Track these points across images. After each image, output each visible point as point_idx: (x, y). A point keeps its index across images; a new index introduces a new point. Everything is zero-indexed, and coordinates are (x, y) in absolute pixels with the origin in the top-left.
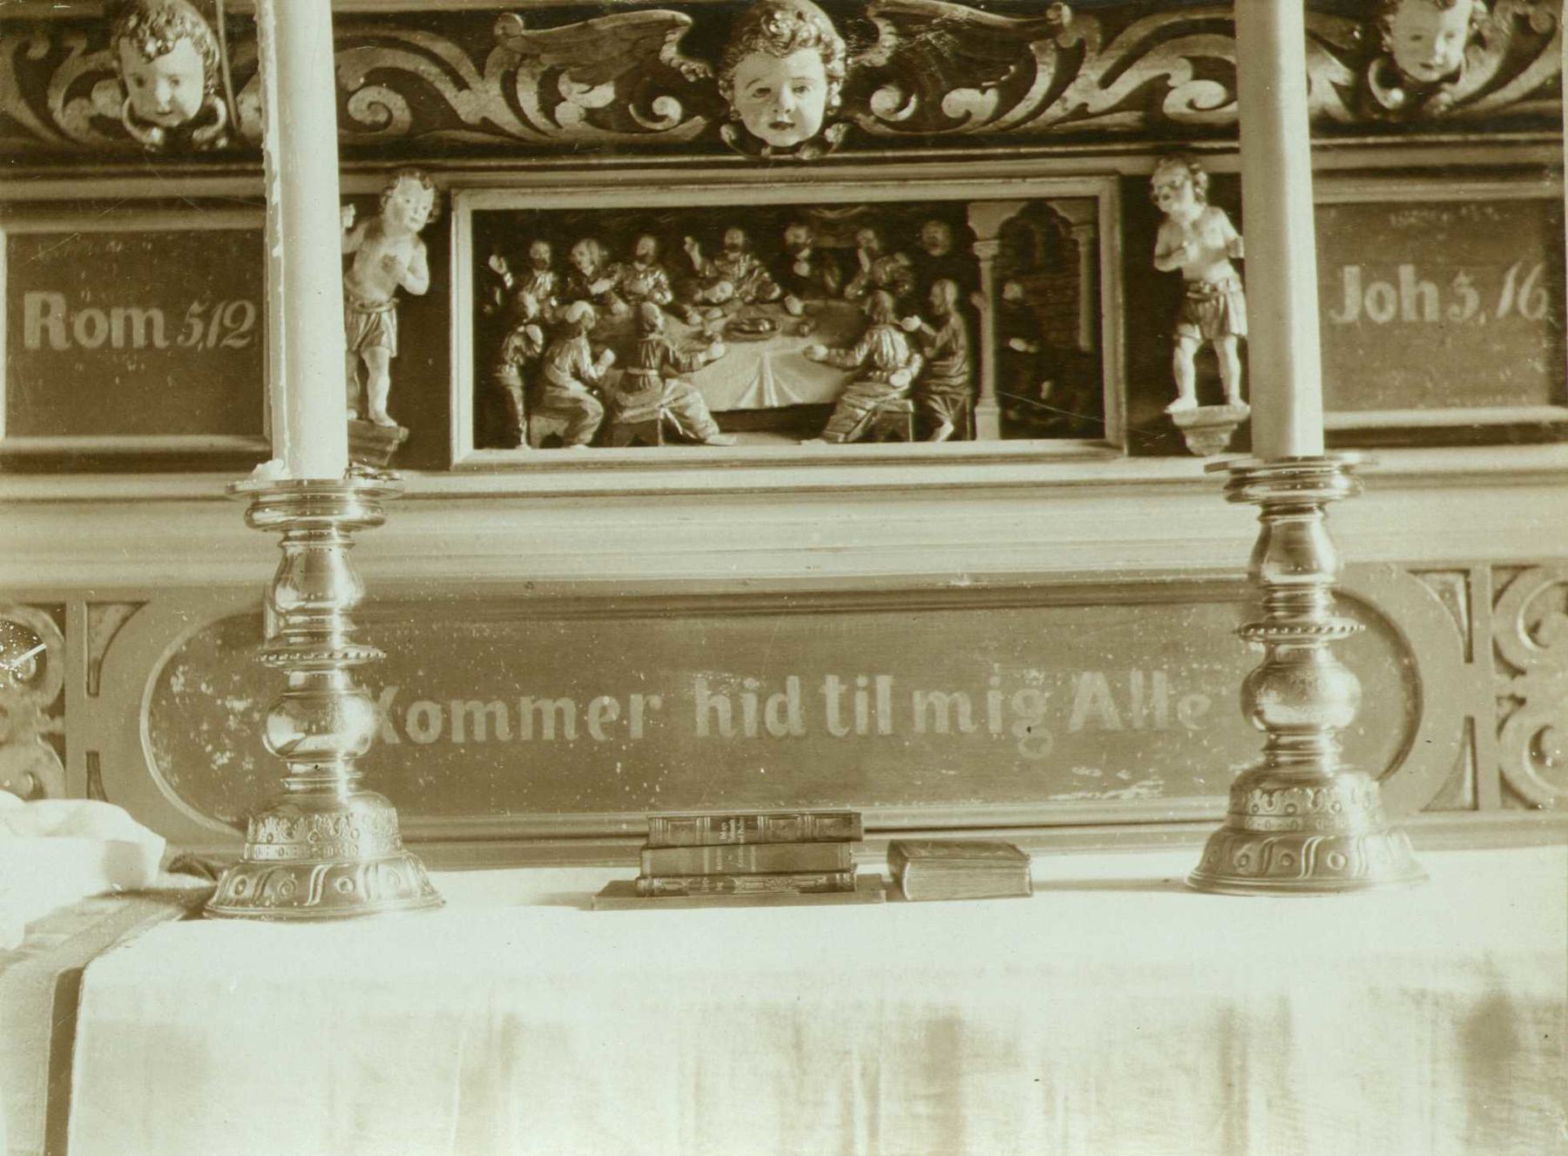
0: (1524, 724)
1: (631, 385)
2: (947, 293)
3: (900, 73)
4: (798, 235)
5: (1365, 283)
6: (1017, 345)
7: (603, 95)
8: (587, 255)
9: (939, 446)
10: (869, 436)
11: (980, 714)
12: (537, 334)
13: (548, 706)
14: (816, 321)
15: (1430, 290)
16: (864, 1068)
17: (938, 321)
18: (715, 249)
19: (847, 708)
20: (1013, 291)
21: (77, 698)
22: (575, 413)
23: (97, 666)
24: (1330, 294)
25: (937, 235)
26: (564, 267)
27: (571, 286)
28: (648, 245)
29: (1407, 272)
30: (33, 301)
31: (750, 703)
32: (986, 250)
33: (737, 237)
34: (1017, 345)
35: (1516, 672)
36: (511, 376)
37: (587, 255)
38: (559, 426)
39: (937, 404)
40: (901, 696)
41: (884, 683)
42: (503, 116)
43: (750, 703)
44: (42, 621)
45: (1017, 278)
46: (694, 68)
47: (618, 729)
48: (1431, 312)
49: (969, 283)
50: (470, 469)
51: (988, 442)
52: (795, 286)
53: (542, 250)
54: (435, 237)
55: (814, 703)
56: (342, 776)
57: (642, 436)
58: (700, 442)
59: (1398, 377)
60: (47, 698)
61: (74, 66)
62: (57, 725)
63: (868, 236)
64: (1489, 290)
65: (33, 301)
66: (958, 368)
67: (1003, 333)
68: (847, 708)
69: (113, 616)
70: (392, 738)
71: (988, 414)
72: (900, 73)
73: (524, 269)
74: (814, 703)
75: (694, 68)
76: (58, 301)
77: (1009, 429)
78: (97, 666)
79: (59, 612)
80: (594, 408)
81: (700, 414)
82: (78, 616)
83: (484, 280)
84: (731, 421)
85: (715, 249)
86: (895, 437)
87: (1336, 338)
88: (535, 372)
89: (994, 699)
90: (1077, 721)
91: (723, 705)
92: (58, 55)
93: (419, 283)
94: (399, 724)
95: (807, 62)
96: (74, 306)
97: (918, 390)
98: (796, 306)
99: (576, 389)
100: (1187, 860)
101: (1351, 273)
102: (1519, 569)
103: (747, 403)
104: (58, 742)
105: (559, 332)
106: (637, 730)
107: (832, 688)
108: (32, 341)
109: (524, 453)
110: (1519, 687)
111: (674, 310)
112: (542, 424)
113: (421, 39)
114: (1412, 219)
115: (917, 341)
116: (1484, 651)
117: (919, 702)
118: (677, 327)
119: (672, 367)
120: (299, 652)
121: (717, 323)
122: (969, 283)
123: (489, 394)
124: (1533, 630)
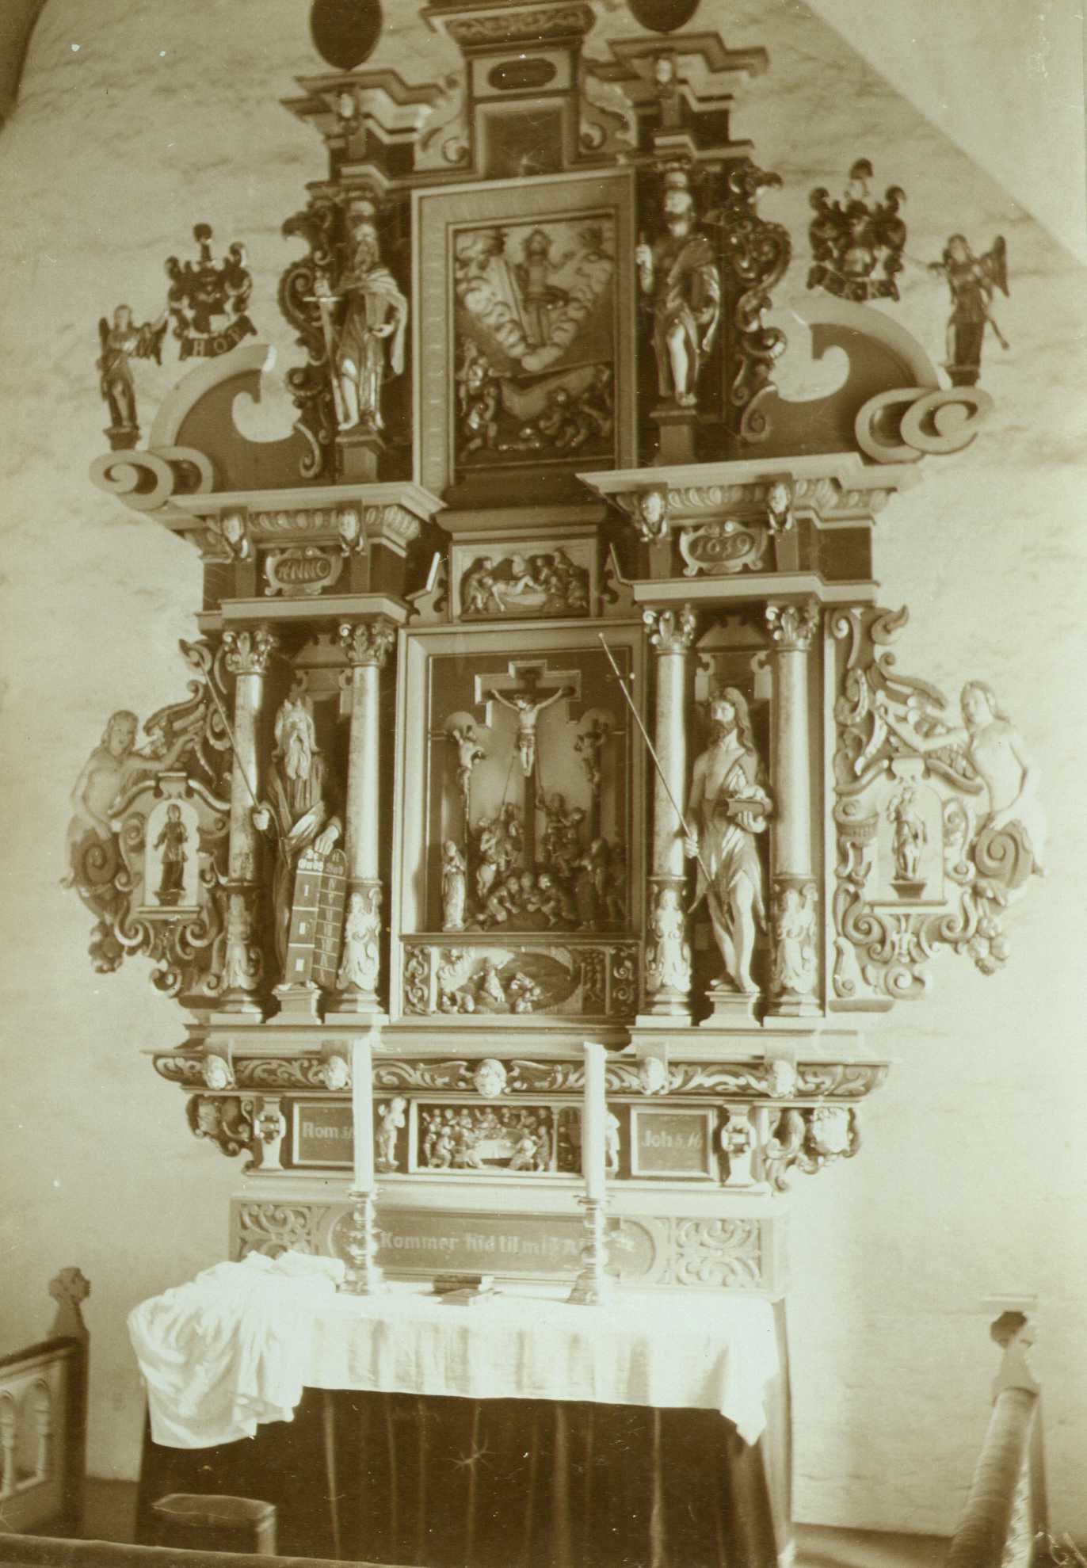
0: (683, 1262)
3: (522, 1078)
4: (505, 1111)
5: (652, 1134)
6: (562, 1145)
7: (446, 1080)
8: (449, 1114)
9: (540, 1172)
10: (520, 1169)
11: (540, 1249)
12: (434, 1137)
14: (509, 1134)
17: (540, 1137)
18: (483, 1113)
19: (506, 1244)
20: (562, 1130)
21: (314, 1231)
22: (443, 1159)
23: (318, 1223)
24: (642, 1138)
25: (543, 1113)
26: (443, 1116)
29: (663, 1134)
32: (555, 1117)
34: (562, 1145)
35: (680, 1246)
37: (449, 1114)
38: (439, 1162)
39: (539, 1161)
40: (520, 1242)
41: (516, 1239)
42: (421, 1083)
44: (305, 1211)
45: (564, 1126)
46: (469, 1075)
47: (447, 1248)
48: (670, 1145)
49: (550, 1127)
50: (414, 1174)
51: (553, 1172)
54: (406, 1112)
56: (370, 1262)
57: (460, 1166)
59: (660, 1162)
61: (314, 1069)
62: (309, 1238)
64: (686, 1139)
65: (305, 1124)
66: (546, 1150)
67: (559, 1141)
68: (506, 1244)
69: (322, 1210)
70: (390, 1246)
71: (553, 1163)
72: (522, 1078)
73: (432, 1116)
74: (497, 1243)
75: (469, 1075)
76: (311, 1125)
77: (561, 1168)
78: (318, 1223)
80: (448, 1156)
81: (477, 1159)
82: (314, 1209)
83: (421, 1120)
84: (486, 1162)
85: (483, 1113)
86: (528, 1169)
87: (643, 1151)
88: (434, 1146)
89: (544, 1246)
92: (311, 1066)
94: (392, 1242)
96: (315, 1126)
97: (534, 1157)
98: (504, 1130)
100: (566, 1293)
101: (648, 1133)
104: (308, 1242)
105: (439, 1135)
106: (452, 1247)
108: (305, 1135)
111: (471, 1130)
112: (435, 1161)
113: (400, 1064)
114: (665, 1118)
115: (535, 1143)
121: (483, 1133)
122: (550, 1127)
124: (687, 1236)
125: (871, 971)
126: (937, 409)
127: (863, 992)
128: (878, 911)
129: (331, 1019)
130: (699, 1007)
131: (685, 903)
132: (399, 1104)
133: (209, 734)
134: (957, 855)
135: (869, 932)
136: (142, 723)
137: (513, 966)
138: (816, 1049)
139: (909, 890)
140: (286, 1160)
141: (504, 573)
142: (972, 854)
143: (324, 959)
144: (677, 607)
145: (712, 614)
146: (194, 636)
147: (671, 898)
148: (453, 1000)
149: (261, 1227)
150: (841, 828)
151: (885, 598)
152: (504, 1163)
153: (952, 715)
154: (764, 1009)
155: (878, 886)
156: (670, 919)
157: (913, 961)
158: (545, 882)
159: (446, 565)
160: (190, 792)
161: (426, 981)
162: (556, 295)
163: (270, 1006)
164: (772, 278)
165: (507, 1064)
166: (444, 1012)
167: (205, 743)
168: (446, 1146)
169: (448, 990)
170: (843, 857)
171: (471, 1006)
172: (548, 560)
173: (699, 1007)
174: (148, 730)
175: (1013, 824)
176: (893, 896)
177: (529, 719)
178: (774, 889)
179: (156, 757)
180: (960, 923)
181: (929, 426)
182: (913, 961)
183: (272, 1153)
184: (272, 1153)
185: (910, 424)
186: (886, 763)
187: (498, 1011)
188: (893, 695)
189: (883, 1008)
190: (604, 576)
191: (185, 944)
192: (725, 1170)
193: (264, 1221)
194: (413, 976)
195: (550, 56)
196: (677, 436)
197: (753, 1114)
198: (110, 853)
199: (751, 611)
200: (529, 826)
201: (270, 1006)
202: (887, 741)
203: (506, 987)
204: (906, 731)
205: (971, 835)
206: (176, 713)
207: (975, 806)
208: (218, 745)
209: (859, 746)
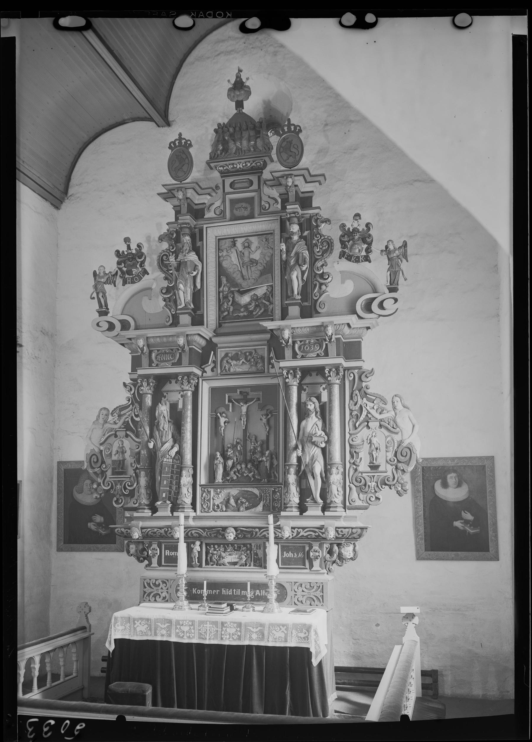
0: (297, 597)
1: (219, 560)
2: (249, 552)
4: (236, 545)
9: (247, 567)
10: (241, 566)
13: (209, 591)
15: (292, 554)
16: (177, 591)
22: (214, 562)
26: (214, 547)
27: (215, 550)
28: (222, 546)
30: (166, 551)
31: (227, 591)
33: (230, 545)
35: (296, 592)
36: (209, 558)
37: (216, 547)
38: (213, 563)
39: (247, 563)
43: (227, 591)
51: (252, 567)
52: (235, 550)
53: (212, 546)
54: (201, 546)
55: (233, 592)
58: (226, 565)
60: (167, 588)
63: (242, 546)
69: (172, 581)
73: (210, 547)
74: (233, 592)
79: (168, 580)
80: (216, 562)
82: (169, 581)
86: (243, 566)
88: (211, 558)
90: (256, 595)
91: (225, 591)
93: (199, 550)
95: (231, 534)
96: (170, 552)
97: (246, 561)
98: (235, 552)
99: (215, 560)
102: (297, 582)
103: (231, 561)
104: (167, 592)
107: (235, 590)
108: (166, 555)
109: (210, 566)
110: (296, 593)
112: (211, 563)
115: (246, 556)
116: (293, 590)
117: (242, 592)
118: (224, 554)
119: (223, 558)
120: (258, 538)
123: (206, 560)
125: (361, 495)
127: (358, 503)
128: (364, 475)
130: (302, 508)
131: (297, 472)
132: (198, 543)
133: (133, 416)
134: (390, 455)
135: (361, 482)
136: (111, 412)
138: (341, 523)
139: (374, 467)
140: (160, 564)
142: (396, 455)
144: (294, 369)
145: (306, 371)
146: (128, 381)
147: (292, 470)
148: (218, 506)
150: (351, 446)
151: (366, 366)
153: (389, 406)
154: (324, 509)
155: (364, 466)
156: (292, 478)
157: (376, 492)
158: (249, 466)
159: (215, 354)
160: (127, 436)
161: (209, 500)
162: (253, 262)
163: (154, 510)
165: (236, 529)
166: (215, 511)
168: (215, 558)
170: (352, 456)
172: (251, 353)
173: (302, 508)
176: (369, 469)
177: (244, 409)
178: (327, 471)
179: (115, 423)
180: (391, 479)
181: (381, 306)
183: (155, 561)
184: (155, 561)
185: (375, 306)
188: (369, 400)
189: (366, 508)
190: (270, 359)
191: (125, 488)
192: (311, 566)
195: (251, 177)
196: (294, 310)
197: (321, 546)
199: (320, 370)
200: (245, 446)
201: (154, 510)
202: (367, 415)
204: (373, 412)
206: (122, 408)
207: (397, 438)
209: (358, 418)
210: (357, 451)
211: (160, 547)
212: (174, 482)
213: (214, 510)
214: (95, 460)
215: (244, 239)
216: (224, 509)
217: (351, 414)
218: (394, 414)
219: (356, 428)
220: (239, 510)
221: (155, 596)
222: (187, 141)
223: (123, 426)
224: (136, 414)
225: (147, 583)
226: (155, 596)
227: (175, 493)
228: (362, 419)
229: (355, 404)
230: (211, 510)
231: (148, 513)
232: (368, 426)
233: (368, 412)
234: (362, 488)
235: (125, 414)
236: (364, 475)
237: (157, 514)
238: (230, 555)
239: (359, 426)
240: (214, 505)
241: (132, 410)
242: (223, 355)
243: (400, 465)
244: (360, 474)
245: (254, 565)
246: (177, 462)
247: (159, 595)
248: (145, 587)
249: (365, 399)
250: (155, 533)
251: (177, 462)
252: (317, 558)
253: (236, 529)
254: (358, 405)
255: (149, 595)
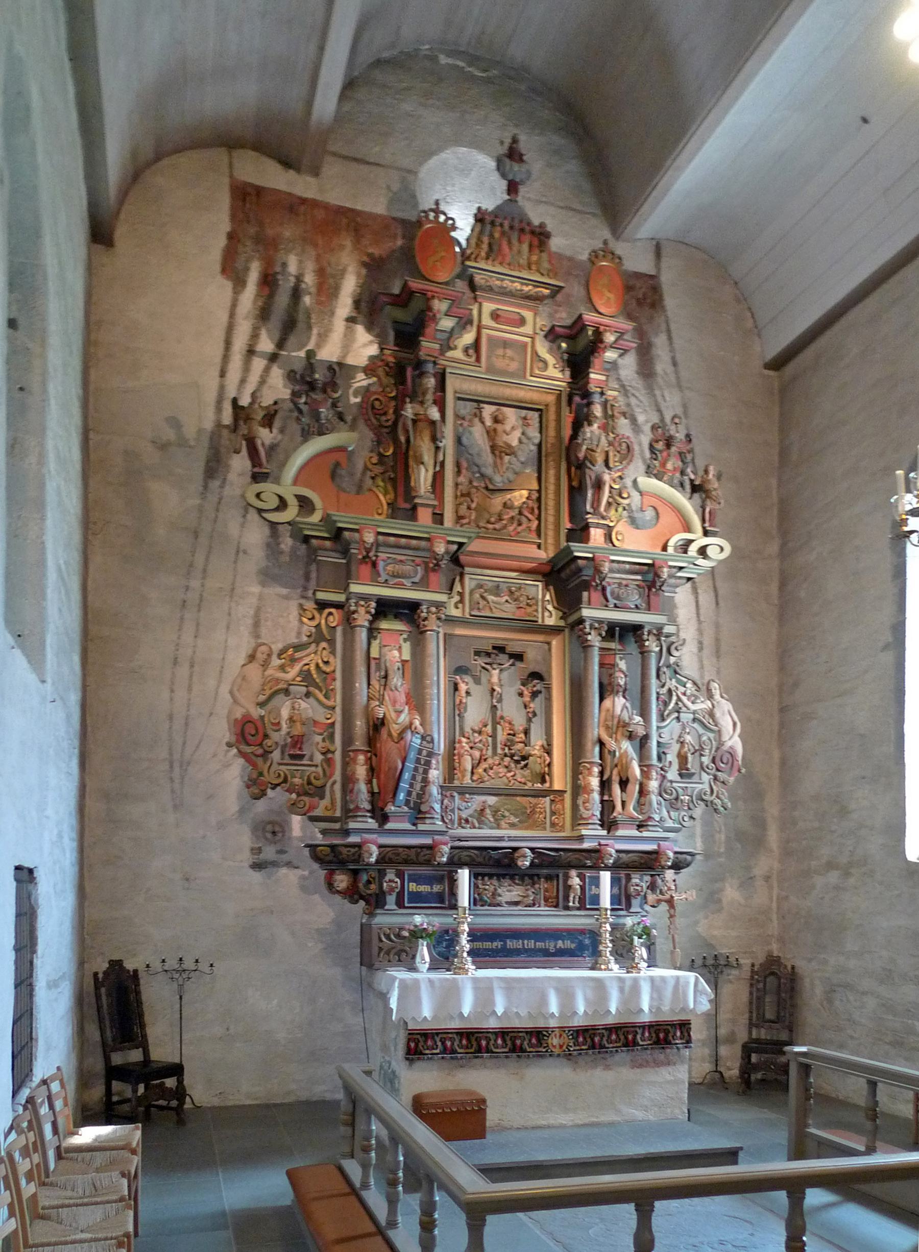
55: (523, 944)
74: (523, 944)
107: (526, 942)
125: (672, 813)
126: (707, 546)
128: (674, 785)
129: (421, 827)
133: (320, 661)
135: (671, 794)
137: (498, 804)
141: (496, 591)
142: (714, 761)
143: (414, 794)
148: (467, 821)
149: (391, 940)
152: (517, 903)
157: (689, 809)
160: (308, 695)
161: (453, 811)
163: (383, 818)
164: (33, 459)
166: (463, 828)
167: (317, 665)
169: (464, 816)
171: (477, 825)
174: (279, 656)
175: (731, 747)
176: (679, 779)
180: (709, 793)
182: (689, 809)
184: (391, 899)
186: (676, 715)
187: (491, 828)
188: (678, 681)
193: (392, 937)
194: (446, 807)
198: (259, 724)
201: (383, 818)
202: (677, 704)
203: (494, 816)
205: (713, 752)
208: (327, 669)
209: (666, 704)
210: (666, 751)
211: (400, 875)
212: (419, 778)
213: (460, 824)
214: (253, 732)
215: (494, 408)
216: (477, 825)
217: (658, 699)
218: (710, 706)
219: (663, 720)
220: (499, 827)
221: (398, 954)
222: (448, 219)
223: (299, 679)
224: (325, 660)
225: (384, 934)
226: (398, 954)
227: (418, 794)
228: (672, 705)
229: (663, 686)
230: (456, 825)
231: (372, 823)
232: (678, 718)
233: (679, 699)
234: (674, 803)
235: (300, 659)
236: (674, 785)
237: (389, 826)
238: (509, 891)
239: (668, 715)
240: (460, 819)
241: (315, 653)
242: (473, 586)
243: (719, 774)
244: (669, 784)
245: (546, 905)
246: (428, 745)
247: (405, 951)
248: (381, 941)
249: (674, 680)
250: (398, 854)
251: (428, 745)
252: (639, 895)
253: (532, 849)
254: (666, 688)
255: (388, 953)
